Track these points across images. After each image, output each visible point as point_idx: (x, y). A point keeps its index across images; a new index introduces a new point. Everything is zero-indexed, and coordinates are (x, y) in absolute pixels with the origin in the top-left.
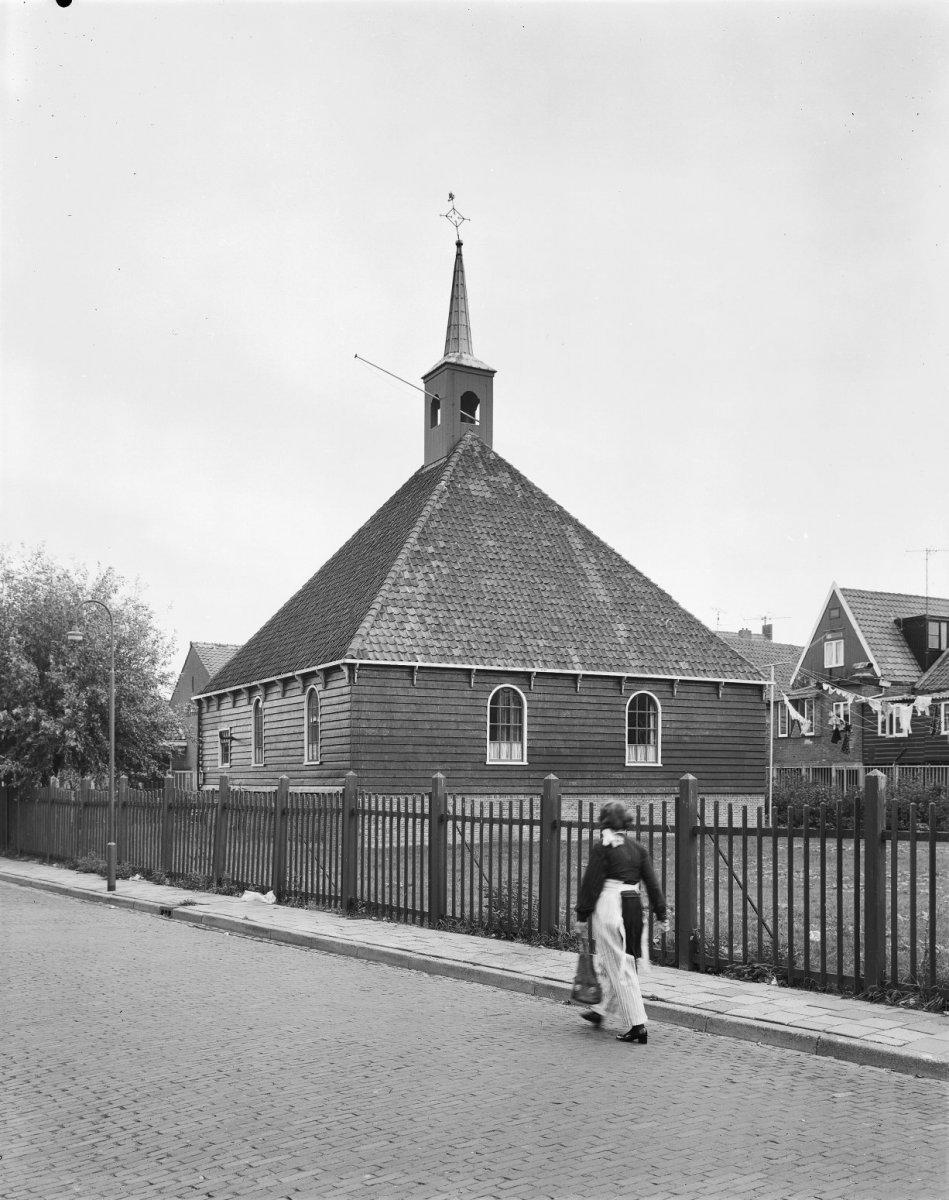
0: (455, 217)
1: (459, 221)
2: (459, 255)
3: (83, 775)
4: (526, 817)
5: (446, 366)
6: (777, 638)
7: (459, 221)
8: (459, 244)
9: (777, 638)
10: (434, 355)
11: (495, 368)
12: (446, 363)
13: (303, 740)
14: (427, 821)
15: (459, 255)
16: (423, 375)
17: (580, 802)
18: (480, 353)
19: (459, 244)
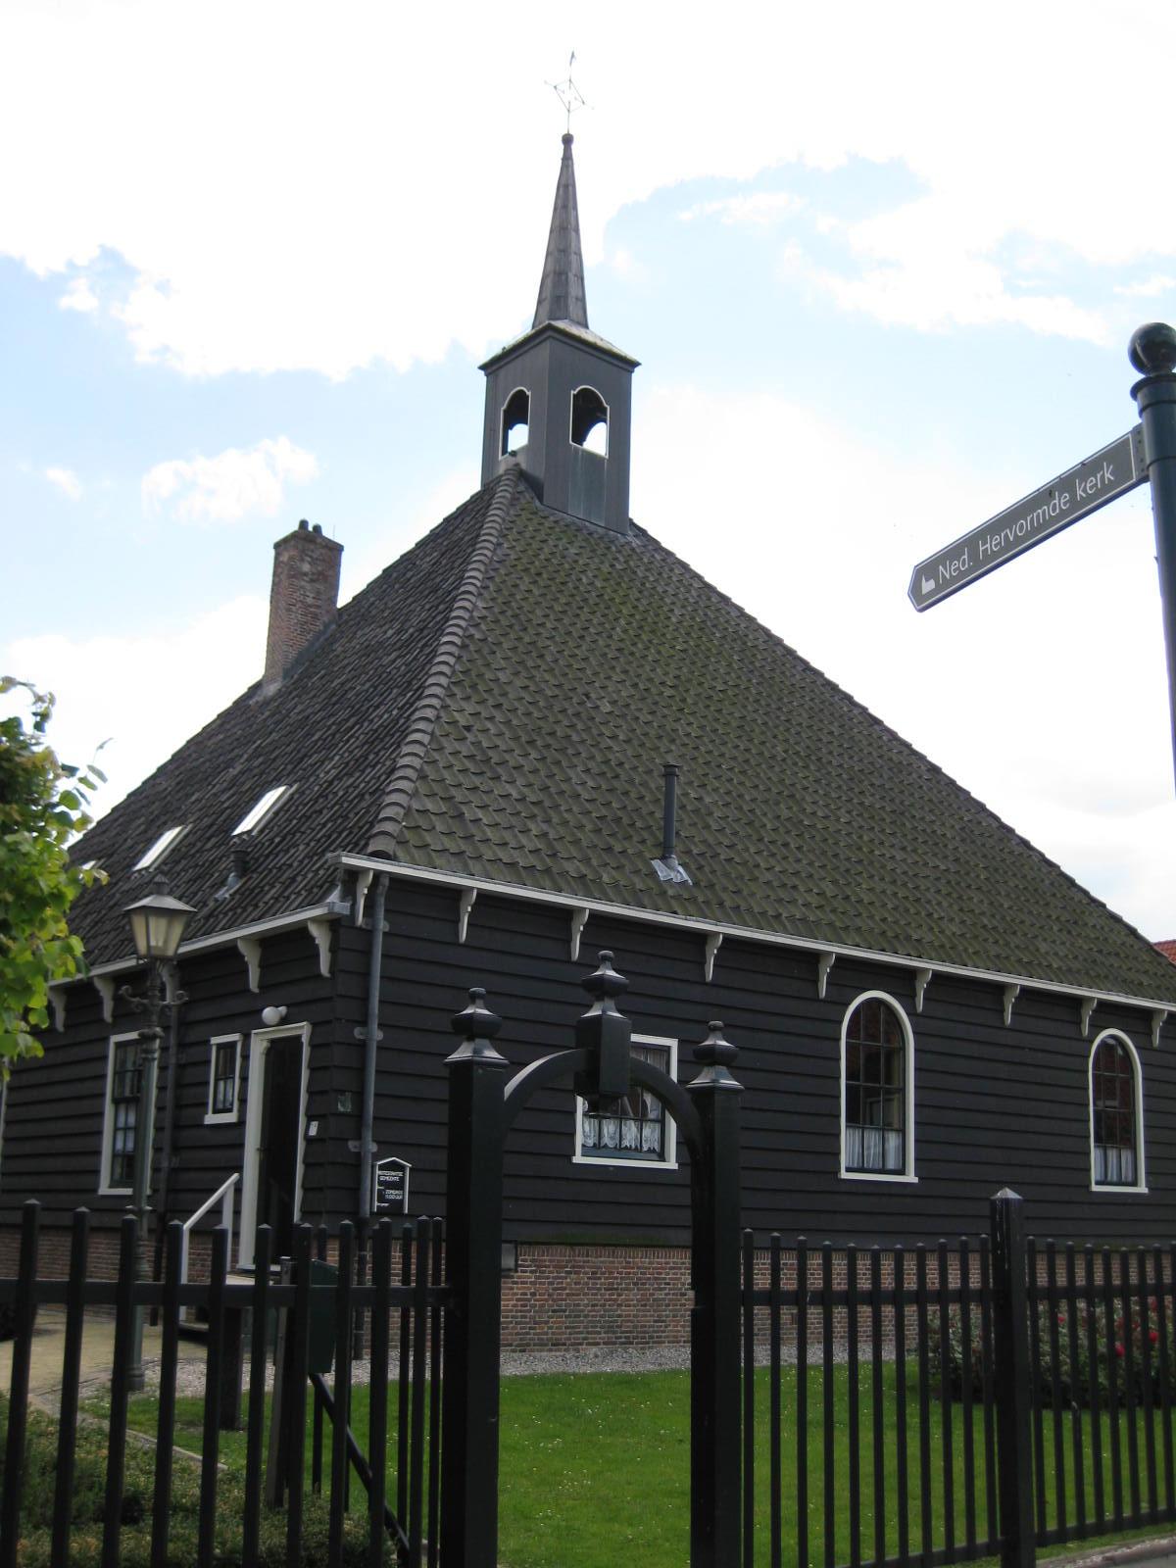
2: (567, 159)
8: (567, 140)
10: (516, 321)
15: (567, 159)
16: (485, 358)
19: (567, 140)
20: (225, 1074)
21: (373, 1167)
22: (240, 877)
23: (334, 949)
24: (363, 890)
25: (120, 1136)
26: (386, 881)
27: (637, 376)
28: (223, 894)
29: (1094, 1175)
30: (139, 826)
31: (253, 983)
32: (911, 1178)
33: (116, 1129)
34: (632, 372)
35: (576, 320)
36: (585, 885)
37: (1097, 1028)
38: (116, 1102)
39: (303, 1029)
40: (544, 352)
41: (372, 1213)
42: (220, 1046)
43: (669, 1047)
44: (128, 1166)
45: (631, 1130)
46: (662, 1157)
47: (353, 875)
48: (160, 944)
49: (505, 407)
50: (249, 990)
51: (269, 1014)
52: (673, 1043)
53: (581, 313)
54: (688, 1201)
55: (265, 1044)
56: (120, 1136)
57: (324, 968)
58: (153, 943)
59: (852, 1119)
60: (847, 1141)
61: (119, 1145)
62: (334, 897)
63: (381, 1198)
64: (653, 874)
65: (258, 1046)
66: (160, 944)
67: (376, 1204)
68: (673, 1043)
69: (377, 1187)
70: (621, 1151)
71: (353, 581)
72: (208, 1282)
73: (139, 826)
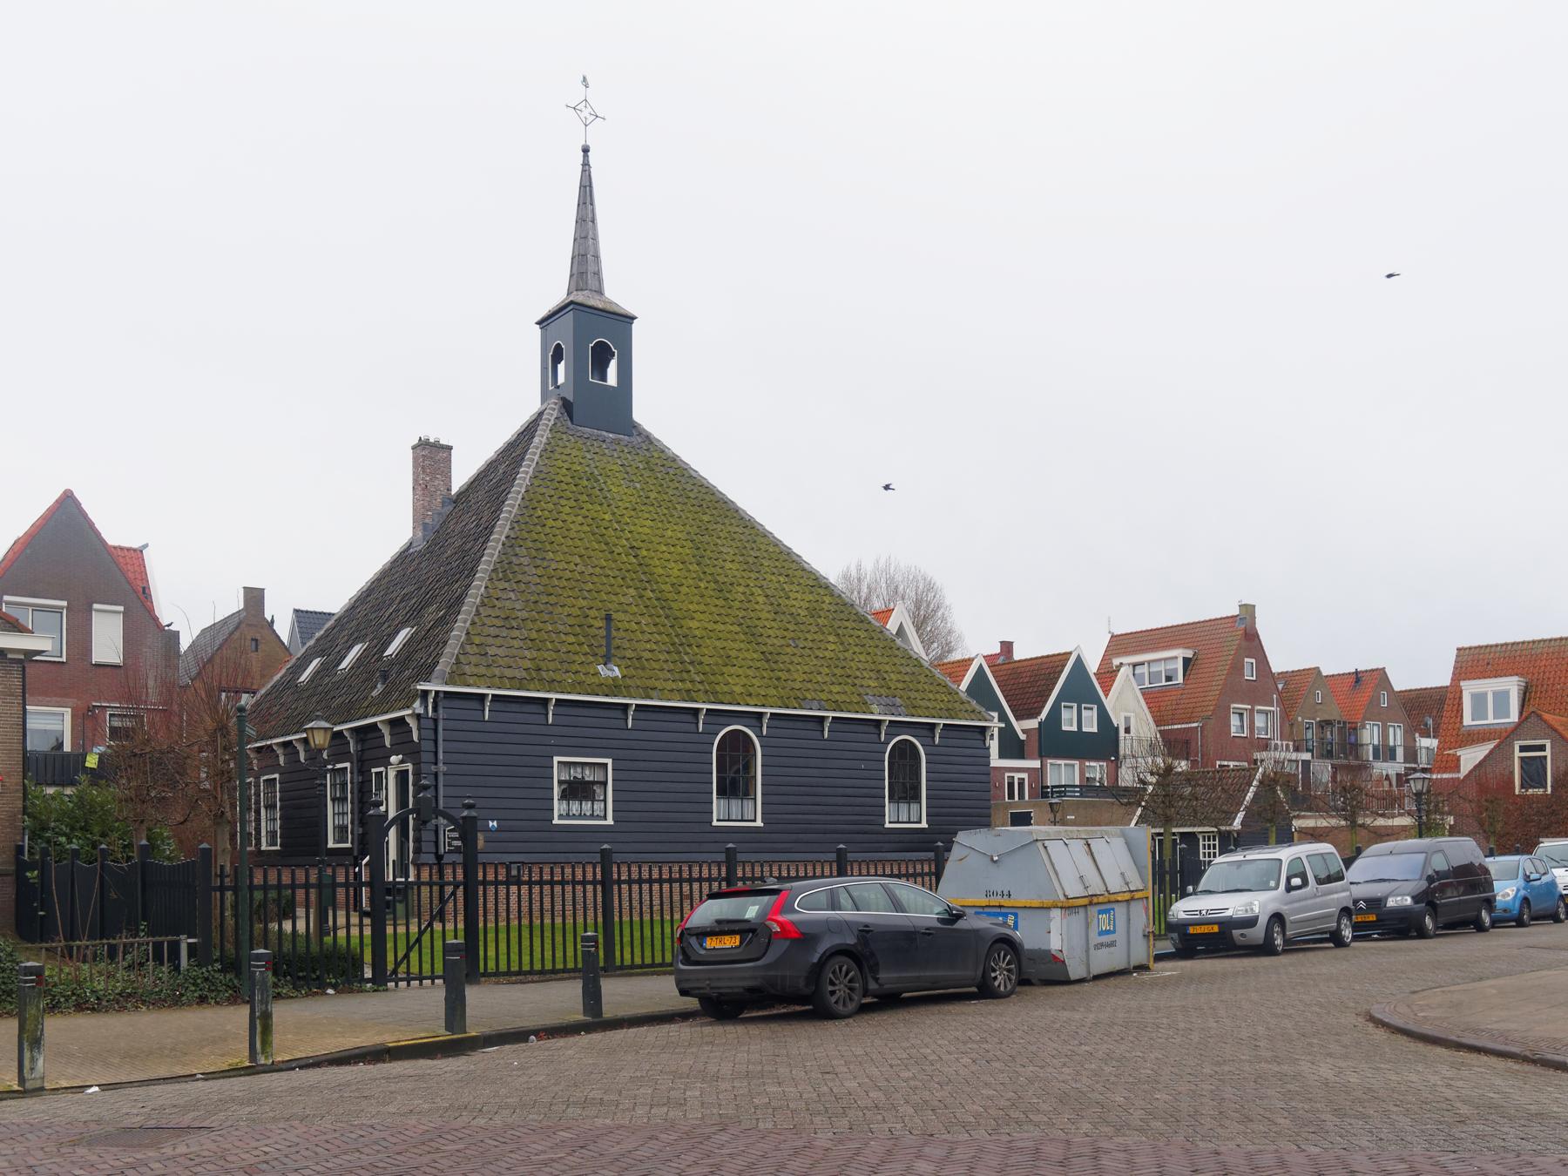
0: (586, 113)
1: (581, 106)
2: (586, 165)
3: (1413, 898)
4: (646, 887)
5: (571, 307)
6: (1018, 655)
7: (581, 106)
8: (586, 150)
9: (1018, 655)
10: (556, 291)
11: (636, 314)
12: (572, 303)
13: (1147, 898)
14: (599, 888)
15: (586, 165)
16: (539, 317)
17: (788, 866)
18: (617, 291)
19: (586, 150)
20: (379, 788)
21: (444, 831)
22: (383, 684)
23: (419, 729)
24: (431, 700)
25: (336, 817)
26: (442, 695)
27: (636, 325)
28: (374, 693)
29: (887, 821)
30: (344, 636)
31: (387, 743)
32: (759, 823)
33: (334, 814)
34: (632, 323)
35: (594, 289)
36: (551, 685)
37: (890, 736)
38: (333, 800)
39: (410, 767)
40: (568, 319)
41: (445, 852)
42: (376, 773)
43: (607, 764)
44: (341, 831)
45: (587, 806)
46: (605, 818)
47: (425, 693)
48: (322, 742)
49: (551, 353)
50: (385, 746)
51: (394, 759)
52: (609, 761)
53: (597, 283)
54: (479, 855)
55: (395, 773)
56: (336, 817)
57: (415, 738)
58: (317, 742)
59: (722, 792)
60: (718, 807)
61: (337, 822)
62: (417, 704)
63: (450, 845)
64: (597, 674)
65: (392, 774)
66: (322, 742)
67: (447, 848)
68: (609, 761)
69: (447, 840)
70: (581, 816)
71: (461, 475)
72: (262, 883)
73: (344, 636)
